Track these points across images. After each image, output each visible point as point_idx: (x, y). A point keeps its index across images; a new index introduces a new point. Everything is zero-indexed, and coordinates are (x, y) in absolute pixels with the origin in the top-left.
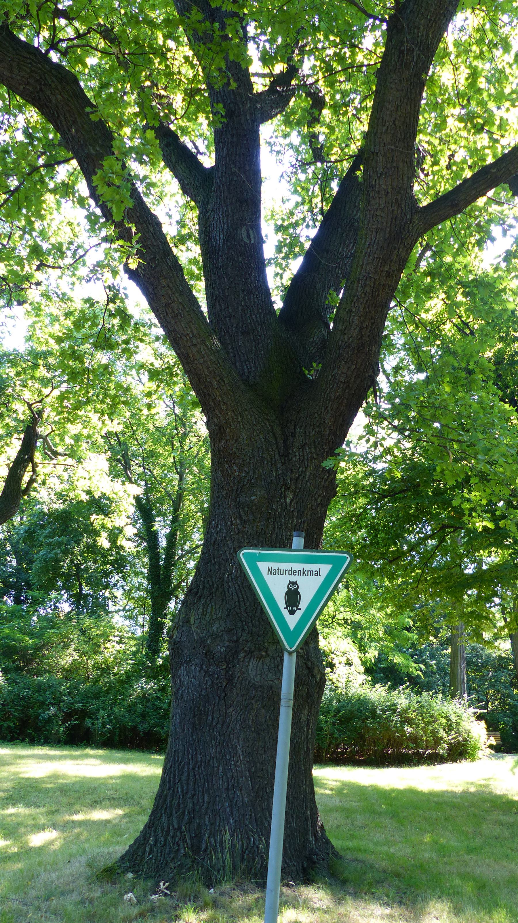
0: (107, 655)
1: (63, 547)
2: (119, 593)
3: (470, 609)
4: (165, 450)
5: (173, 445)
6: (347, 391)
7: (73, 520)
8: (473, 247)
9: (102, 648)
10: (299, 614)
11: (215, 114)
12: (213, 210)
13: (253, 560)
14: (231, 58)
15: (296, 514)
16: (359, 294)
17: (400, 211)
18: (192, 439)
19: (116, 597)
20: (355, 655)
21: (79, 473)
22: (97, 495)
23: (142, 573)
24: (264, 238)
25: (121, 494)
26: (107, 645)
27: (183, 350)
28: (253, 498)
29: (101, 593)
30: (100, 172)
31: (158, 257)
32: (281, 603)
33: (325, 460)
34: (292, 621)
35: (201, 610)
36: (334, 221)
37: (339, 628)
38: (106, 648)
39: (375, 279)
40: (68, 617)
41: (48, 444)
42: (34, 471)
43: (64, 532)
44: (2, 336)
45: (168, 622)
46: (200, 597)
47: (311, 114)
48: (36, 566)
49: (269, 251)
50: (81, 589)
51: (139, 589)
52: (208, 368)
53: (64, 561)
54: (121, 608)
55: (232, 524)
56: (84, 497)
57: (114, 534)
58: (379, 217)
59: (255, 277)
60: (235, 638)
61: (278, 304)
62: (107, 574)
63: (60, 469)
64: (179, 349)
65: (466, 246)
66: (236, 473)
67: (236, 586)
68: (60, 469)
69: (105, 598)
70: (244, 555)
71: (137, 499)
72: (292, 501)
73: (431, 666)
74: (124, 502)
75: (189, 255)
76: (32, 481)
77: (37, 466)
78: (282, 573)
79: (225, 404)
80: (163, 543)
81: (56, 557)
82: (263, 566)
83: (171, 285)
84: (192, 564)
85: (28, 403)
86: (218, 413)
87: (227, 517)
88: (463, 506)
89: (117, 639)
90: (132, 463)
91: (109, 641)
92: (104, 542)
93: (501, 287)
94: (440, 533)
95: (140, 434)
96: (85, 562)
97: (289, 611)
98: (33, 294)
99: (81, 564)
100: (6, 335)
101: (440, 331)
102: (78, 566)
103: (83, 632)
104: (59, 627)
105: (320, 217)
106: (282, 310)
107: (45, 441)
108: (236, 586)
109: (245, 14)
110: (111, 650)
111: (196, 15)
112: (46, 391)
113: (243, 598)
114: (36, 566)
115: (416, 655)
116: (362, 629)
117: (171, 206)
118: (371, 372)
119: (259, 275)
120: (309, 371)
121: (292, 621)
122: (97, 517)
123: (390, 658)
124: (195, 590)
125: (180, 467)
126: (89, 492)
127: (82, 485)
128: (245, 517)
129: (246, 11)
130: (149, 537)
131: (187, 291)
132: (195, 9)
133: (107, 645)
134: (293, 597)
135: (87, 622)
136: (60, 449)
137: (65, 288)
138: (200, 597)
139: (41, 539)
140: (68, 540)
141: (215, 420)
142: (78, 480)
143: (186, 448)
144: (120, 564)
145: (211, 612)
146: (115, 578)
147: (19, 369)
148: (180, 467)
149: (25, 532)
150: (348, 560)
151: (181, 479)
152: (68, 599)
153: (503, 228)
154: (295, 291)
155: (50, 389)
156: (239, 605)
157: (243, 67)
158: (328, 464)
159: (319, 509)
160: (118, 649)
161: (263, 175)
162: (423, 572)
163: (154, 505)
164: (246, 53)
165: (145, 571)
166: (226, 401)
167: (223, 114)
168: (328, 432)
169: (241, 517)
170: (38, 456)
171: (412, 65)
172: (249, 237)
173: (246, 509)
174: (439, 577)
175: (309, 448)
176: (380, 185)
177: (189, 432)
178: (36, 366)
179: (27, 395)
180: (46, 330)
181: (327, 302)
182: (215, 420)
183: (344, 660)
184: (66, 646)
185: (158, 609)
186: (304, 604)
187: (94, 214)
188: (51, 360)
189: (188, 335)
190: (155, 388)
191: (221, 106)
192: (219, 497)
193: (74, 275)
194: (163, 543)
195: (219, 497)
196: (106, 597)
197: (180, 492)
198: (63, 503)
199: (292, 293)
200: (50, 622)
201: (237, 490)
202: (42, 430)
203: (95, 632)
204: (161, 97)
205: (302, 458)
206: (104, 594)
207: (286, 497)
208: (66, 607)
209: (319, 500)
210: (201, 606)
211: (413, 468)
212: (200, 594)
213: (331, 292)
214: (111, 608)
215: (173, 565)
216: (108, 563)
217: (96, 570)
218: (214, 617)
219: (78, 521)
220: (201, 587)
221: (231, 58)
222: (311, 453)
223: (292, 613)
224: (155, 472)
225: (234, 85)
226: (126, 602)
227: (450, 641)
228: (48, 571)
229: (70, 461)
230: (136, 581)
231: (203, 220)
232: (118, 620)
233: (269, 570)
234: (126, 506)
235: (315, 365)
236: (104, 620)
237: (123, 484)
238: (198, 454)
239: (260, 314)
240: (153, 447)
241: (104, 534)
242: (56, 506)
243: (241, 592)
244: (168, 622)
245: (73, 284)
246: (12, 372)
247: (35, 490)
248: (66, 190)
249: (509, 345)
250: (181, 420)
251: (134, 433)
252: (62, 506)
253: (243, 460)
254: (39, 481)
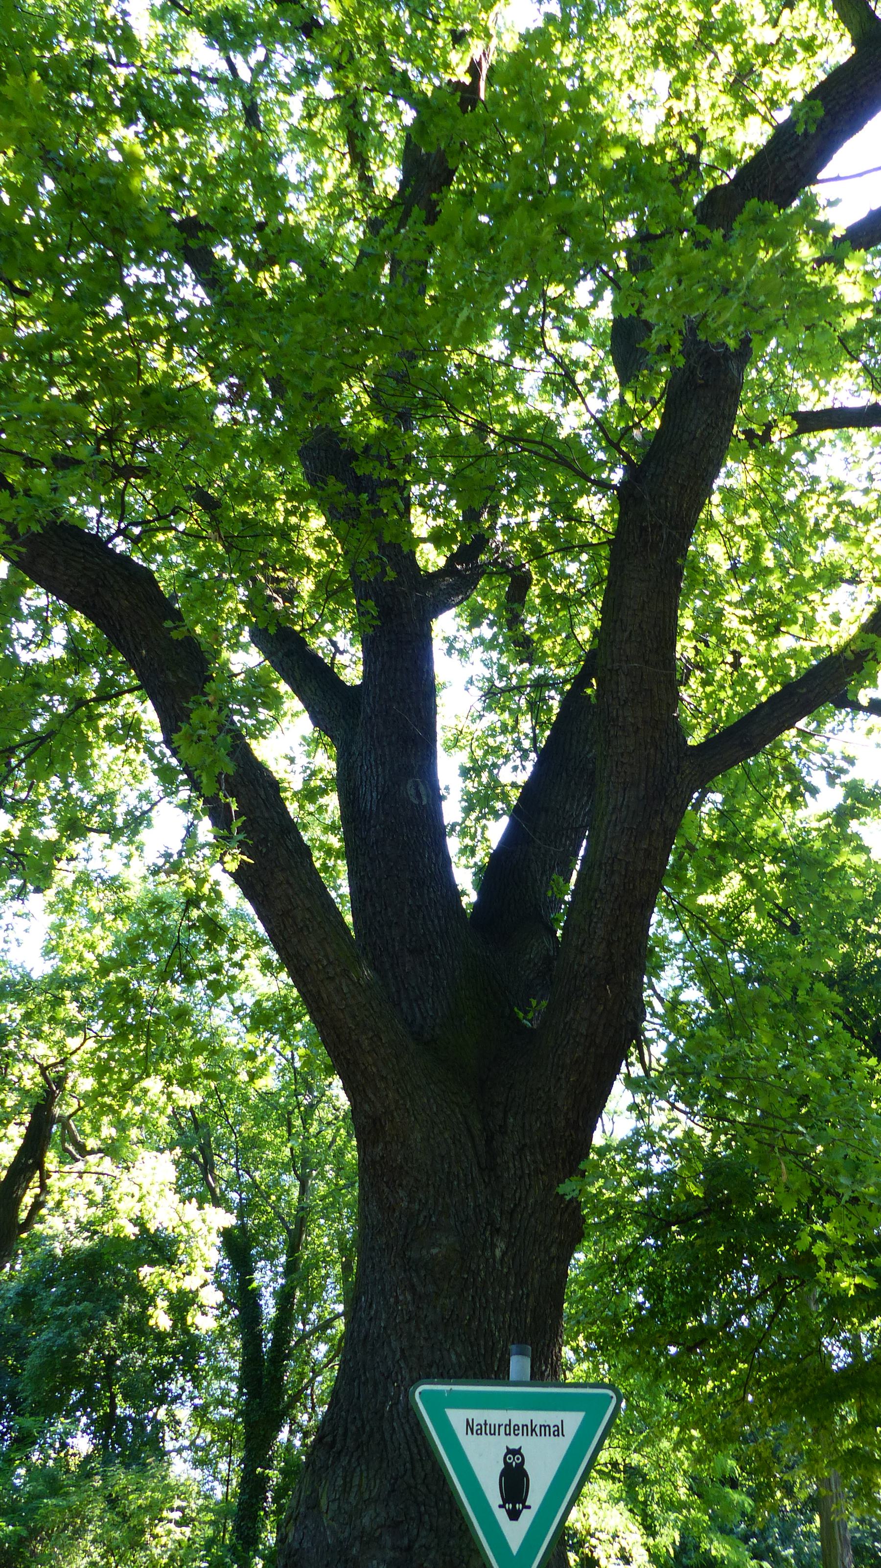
0: (156, 1551)
1: (86, 1323)
2: (183, 1413)
3: (848, 1444)
4: (276, 1135)
5: (290, 1126)
6: (592, 1050)
7: (109, 1269)
8: (783, 803)
9: (147, 1536)
10: (527, 1517)
11: (361, 614)
12: (360, 754)
13: (438, 1405)
14: (387, 538)
15: (512, 1280)
16: (602, 886)
17: (659, 756)
18: (324, 1112)
19: (178, 1423)
20: (634, 1538)
21: (126, 1187)
22: (152, 1227)
23: (229, 1370)
24: (442, 792)
25: (196, 1226)
26: (158, 1530)
27: (310, 987)
28: (434, 1251)
29: (151, 1414)
30: (185, 727)
31: (271, 836)
32: (494, 1497)
33: (563, 1182)
34: (515, 1533)
35: (340, 1482)
36: (557, 760)
37: (602, 1483)
38: (155, 1537)
39: (627, 863)
40: (86, 1471)
41: (71, 1132)
42: (43, 1186)
43: (90, 1293)
44: (6, 947)
45: (274, 1475)
46: (339, 1453)
47: (510, 610)
48: (33, 1361)
49: (451, 811)
50: (113, 1406)
51: (221, 1403)
52: (354, 1017)
53: (86, 1351)
54: (187, 1443)
55: (397, 1302)
56: (131, 1231)
57: (182, 1303)
58: (630, 760)
59: (430, 858)
60: (406, 1541)
61: (470, 898)
62: (164, 1374)
63: (89, 1181)
64: (305, 985)
65: (771, 801)
66: (404, 1204)
67: (407, 1428)
68: (89, 1181)
69: (158, 1426)
70: (423, 1393)
71: (226, 1234)
72: (504, 1254)
73: (786, 1559)
74: (201, 1242)
75: (321, 826)
76: (38, 1204)
77: (49, 1177)
78: (494, 1431)
79: (383, 1078)
80: (269, 1309)
81: (71, 1342)
82: (457, 1417)
83: (292, 880)
84: (320, 1352)
85: (41, 1066)
86: (371, 1095)
87: (387, 1287)
88: (815, 1251)
89: (177, 1515)
90: (216, 1158)
91: (161, 1520)
92: (161, 1319)
93: (836, 863)
94: (775, 1289)
95: (233, 1107)
96: (124, 1352)
97: (508, 1511)
98: (64, 875)
99: (117, 1357)
100: (13, 946)
101: (740, 923)
102: (110, 1360)
103: (112, 1502)
104: (67, 1494)
105: (533, 756)
106: (476, 906)
107: (65, 1126)
108: (407, 1428)
109: (406, 482)
110: (163, 1540)
111: (334, 485)
112: (72, 1043)
113: (419, 1453)
114: (33, 1361)
115: (754, 1535)
116: (645, 1482)
117: (290, 746)
118: (631, 1016)
119: (437, 855)
120: (526, 1013)
121: (515, 1533)
122: (151, 1270)
123: (705, 1545)
124: (329, 1439)
125: (303, 1165)
126: (139, 1222)
127: (127, 1208)
128: (420, 1289)
129: (408, 478)
130: (243, 1299)
131: (318, 891)
132: (331, 480)
133: (158, 1530)
134: (514, 1482)
135: (122, 1478)
136: (91, 1143)
137: (114, 867)
138: (339, 1453)
139: (46, 1308)
140: (96, 1310)
141: (367, 1107)
142: (120, 1200)
143: (313, 1130)
144: (188, 1350)
145: (360, 1486)
146: (178, 1384)
147: (31, 1006)
148: (303, 1165)
149: (18, 1294)
150: (614, 1402)
151: (303, 1190)
152: (87, 1426)
153: (829, 774)
154: (495, 874)
155: (79, 1039)
156: (413, 1468)
157: (406, 550)
158: (568, 1188)
159: (554, 1267)
160: (178, 1536)
161: (439, 680)
162: (751, 1368)
163: (254, 1238)
164: (409, 531)
165: (235, 1365)
166: (384, 1073)
167: (375, 614)
168: (563, 1123)
169: (413, 1288)
170: (51, 1160)
171: (662, 546)
172: (418, 795)
173: (423, 1273)
174: (781, 1378)
175: (532, 1154)
176: (625, 718)
177: (319, 1102)
178: (59, 1001)
179: (40, 1049)
180: (81, 937)
181: (550, 893)
182: (367, 1107)
183: (615, 1549)
184: (79, 1533)
185: (256, 1441)
186: (536, 1496)
187: (169, 767)
188: (86, 992)
189: (319, 961)
190: (261, 1043)
191: (371, 603)
192: (373, 1249)
193: (131, 842)
194: (269, 1309)
195: (373, 1249)
196: (158, 1422)
197: (301, 1214)
198: (91, 1238)
199: (491, 876)
200: (50, 1483)
201: (405, 1236)
202: (64, 1108)
203: (136, 1501)
204: (278, 580)
205: (519, 1172)
206: (155, 1415)
207: (493, 1246)
208: (82, 1445)
209: (553, 1250)
210: (340, 1472)
211: (715, 1170)
212: (338, 1446)
213: (555, 876)
214: (169, 1445)
215: (288, 1357)
216: (167, 1353)
217: (144, 1367)
218: (366, 1496)
219: (117, 1272)
220: (341, 1431)
221: (387, 538)
222: (535, 1162)
223: (514, 1515)
224: (257, 1174)
225: (391, 575)
226: (196, 1429)
227: (815, 1503)
228: (54, 1371)
229: (107, 1165)
230: (217, 1386)
231: (344, 761)
232: (180, 1469)
233: (469, 1426)
234: (204, 1249)
235: (534, 1003)
236: (153, 1476)
237: (200, 1208)
238: (334, 1140)
239: (439, 918)
240: (255, 1130)
241: (162, 1304)
242: (77, 1243)
243: (416, 1441)
244: (274, 1475)
245: (129, 857)
246: (18, 1012)
247: (42, 1221)
248: (130, 729)
249: (859, 947)
250: (305, 1081)
251: (222, 1106)
252: (87, 1244)
253: (416, 1180)
254: (51, 1204)
